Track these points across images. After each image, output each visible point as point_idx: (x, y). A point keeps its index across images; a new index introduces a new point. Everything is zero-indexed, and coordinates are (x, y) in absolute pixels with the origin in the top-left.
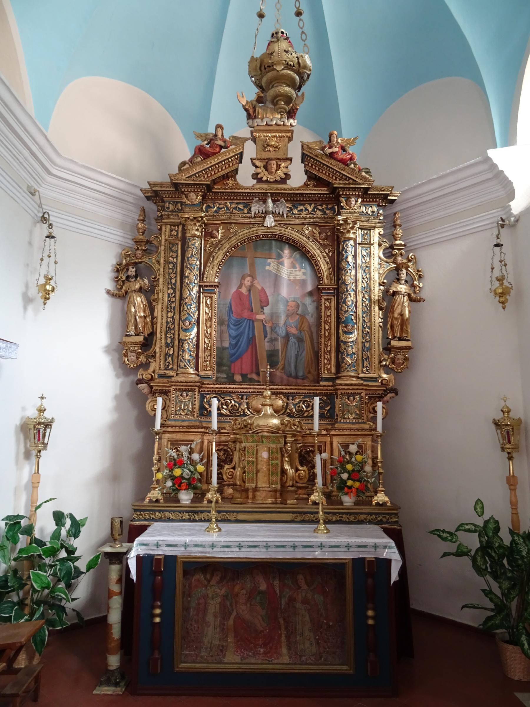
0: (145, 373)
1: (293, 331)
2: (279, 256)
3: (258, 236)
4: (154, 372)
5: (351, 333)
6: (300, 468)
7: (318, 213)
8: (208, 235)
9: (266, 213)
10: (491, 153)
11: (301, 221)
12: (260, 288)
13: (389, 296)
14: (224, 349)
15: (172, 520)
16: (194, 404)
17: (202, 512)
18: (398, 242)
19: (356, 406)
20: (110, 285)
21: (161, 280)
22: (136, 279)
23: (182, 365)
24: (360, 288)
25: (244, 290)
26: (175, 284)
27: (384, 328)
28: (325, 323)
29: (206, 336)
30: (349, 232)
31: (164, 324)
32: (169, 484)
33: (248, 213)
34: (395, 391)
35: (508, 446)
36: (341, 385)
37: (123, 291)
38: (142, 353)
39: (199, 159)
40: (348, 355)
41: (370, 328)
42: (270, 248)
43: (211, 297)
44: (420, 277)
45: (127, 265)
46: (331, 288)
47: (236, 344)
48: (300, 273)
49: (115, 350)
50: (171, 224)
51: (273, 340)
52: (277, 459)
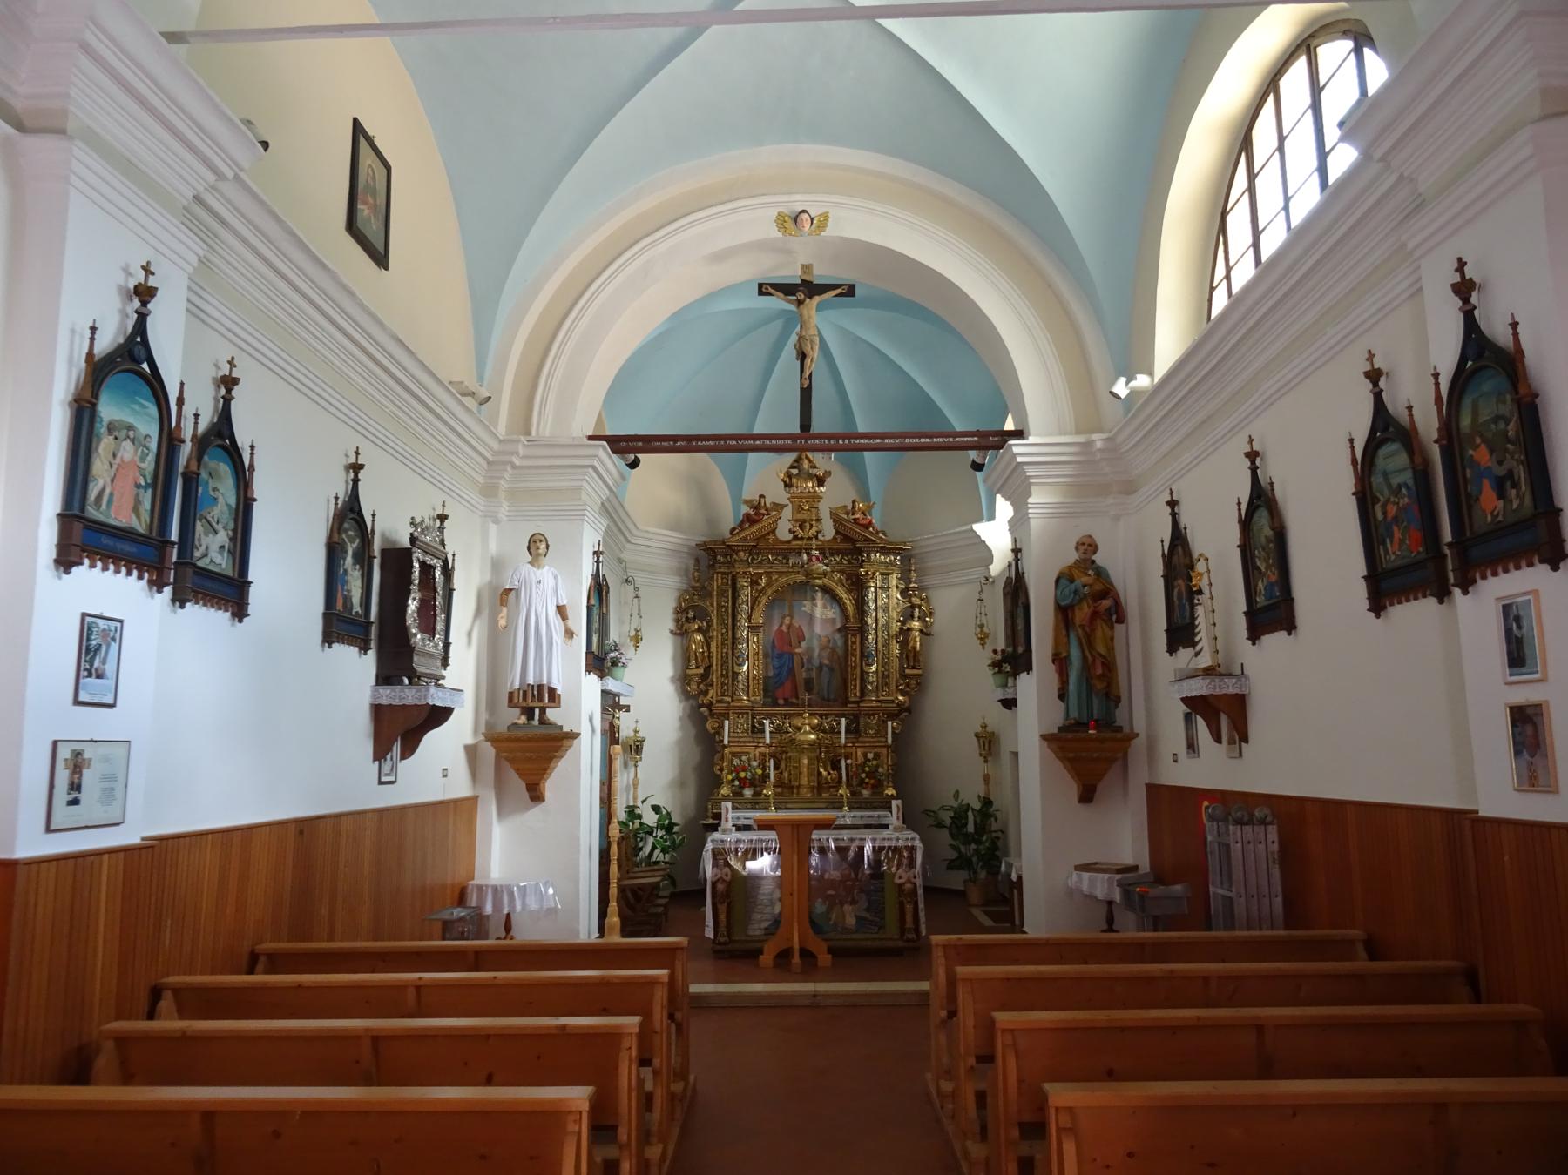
2: (814, 599)
8: (754, 583)
10: (977, 527)
20: (671, 625)
25: (784, 628)
27: (900, 658)
38: (701, 684)
46: (854, 626)
51: (809, 670)
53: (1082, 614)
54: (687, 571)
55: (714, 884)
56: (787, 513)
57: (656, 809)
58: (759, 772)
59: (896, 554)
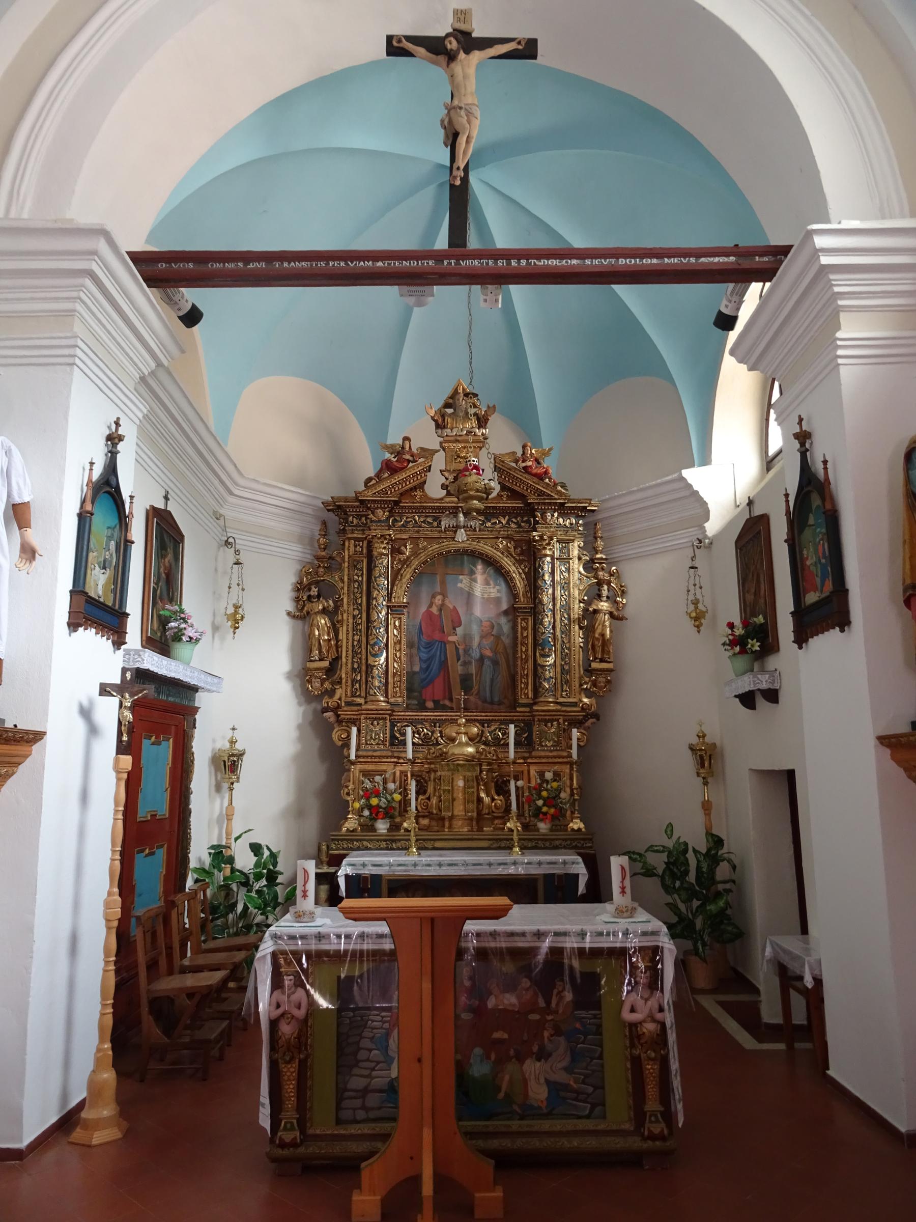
0: (330, 701)
1: (488, 653)
2: (472, 573)
3: (450, 551)
4: (340, 699)
5: (549, 656)
6: (496, 797)
7: (513, 525)
8: (395, 551)
9: (457, 527)
10: (686, 473)
11: (496, 534)
12: (451, 607)
13: (590, 615)
14: (415, 673)
15: (370, 849)
16: (385, 734)
17: (400, 840)
18: (598, 556)
19: (554, 732)
20: (290, 606)
21: (345, 600)
22: (319, 599)
23: (372, 692)
24: (558, 606)
25: (434, 610)
26: (360, 604)
27: (585, 649)
28: (522, 645)
29: (395, 660)
30: (545, 548)
31: (350, 648)
32: (366, 813)
33: (438, 527)
34: (596, 716)
35: (702, 771)
36: (537, 711)
37: (304, 612)
38: (327, 681)
39: (386, 475)
40: (545, 679)
41: (569, 649)
42: (462, 564)
43: (400, 618)
44: (623, 592)
45: (310, 584)
46: (526, 607)
47: (428, 667)
48: (495, 590)
49: (297, 676)
50: (356, 539)
51: (466, 664)
52: (473, 787)
54: (311, 539)
55: (274, 1024)
56: (439, 461)
57: (256, 848)
58: (397, 797)
59: (578, 517)
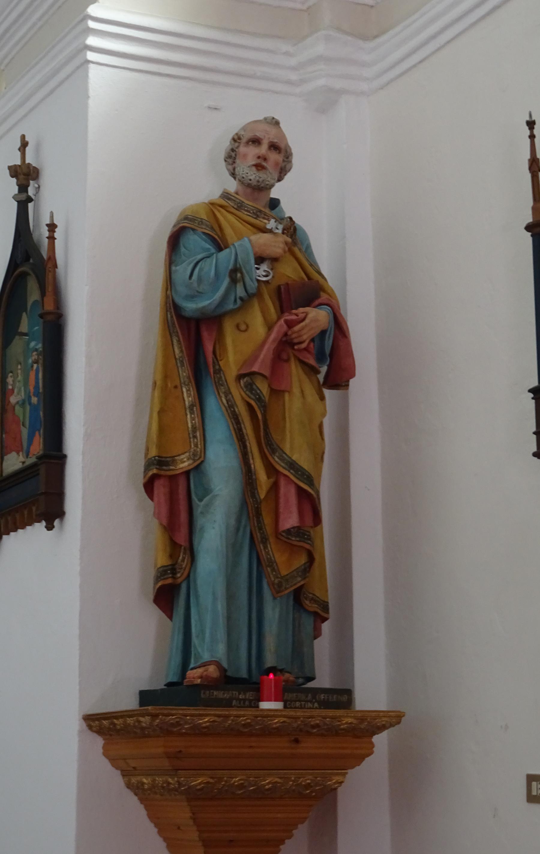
53: (245, 342)
